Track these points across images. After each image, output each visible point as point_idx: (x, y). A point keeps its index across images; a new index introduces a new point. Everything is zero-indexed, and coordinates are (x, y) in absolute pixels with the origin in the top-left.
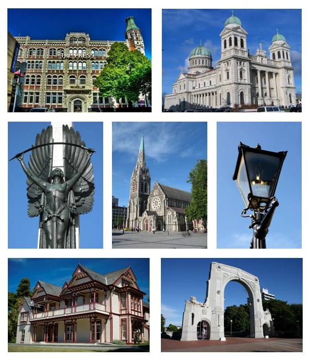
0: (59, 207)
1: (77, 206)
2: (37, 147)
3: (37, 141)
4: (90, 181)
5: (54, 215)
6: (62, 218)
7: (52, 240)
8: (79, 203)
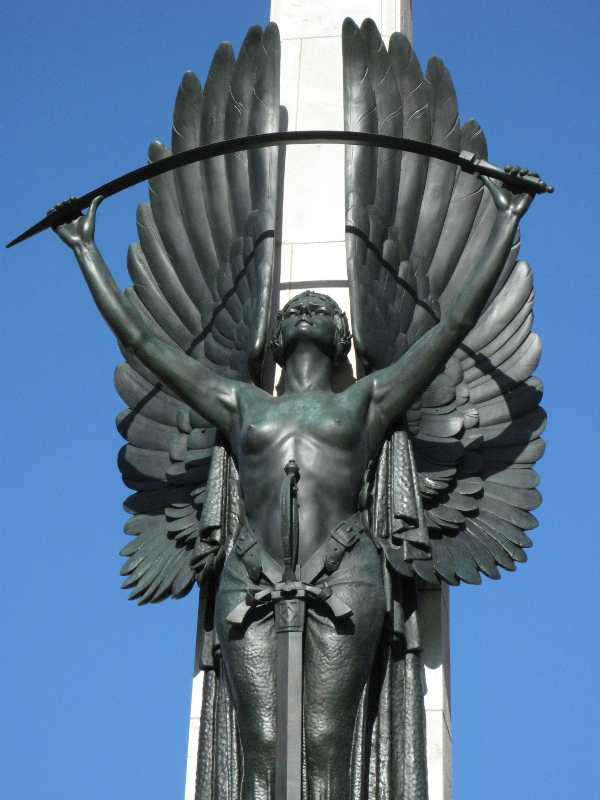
0: (321, 534)
1: (435, 533)
2: (180, 160)
3: (179, 121)
4: (515, 371)
5: (288, 587)
6: (341, 604)
7: (279, 745)
8: (447, 514)
